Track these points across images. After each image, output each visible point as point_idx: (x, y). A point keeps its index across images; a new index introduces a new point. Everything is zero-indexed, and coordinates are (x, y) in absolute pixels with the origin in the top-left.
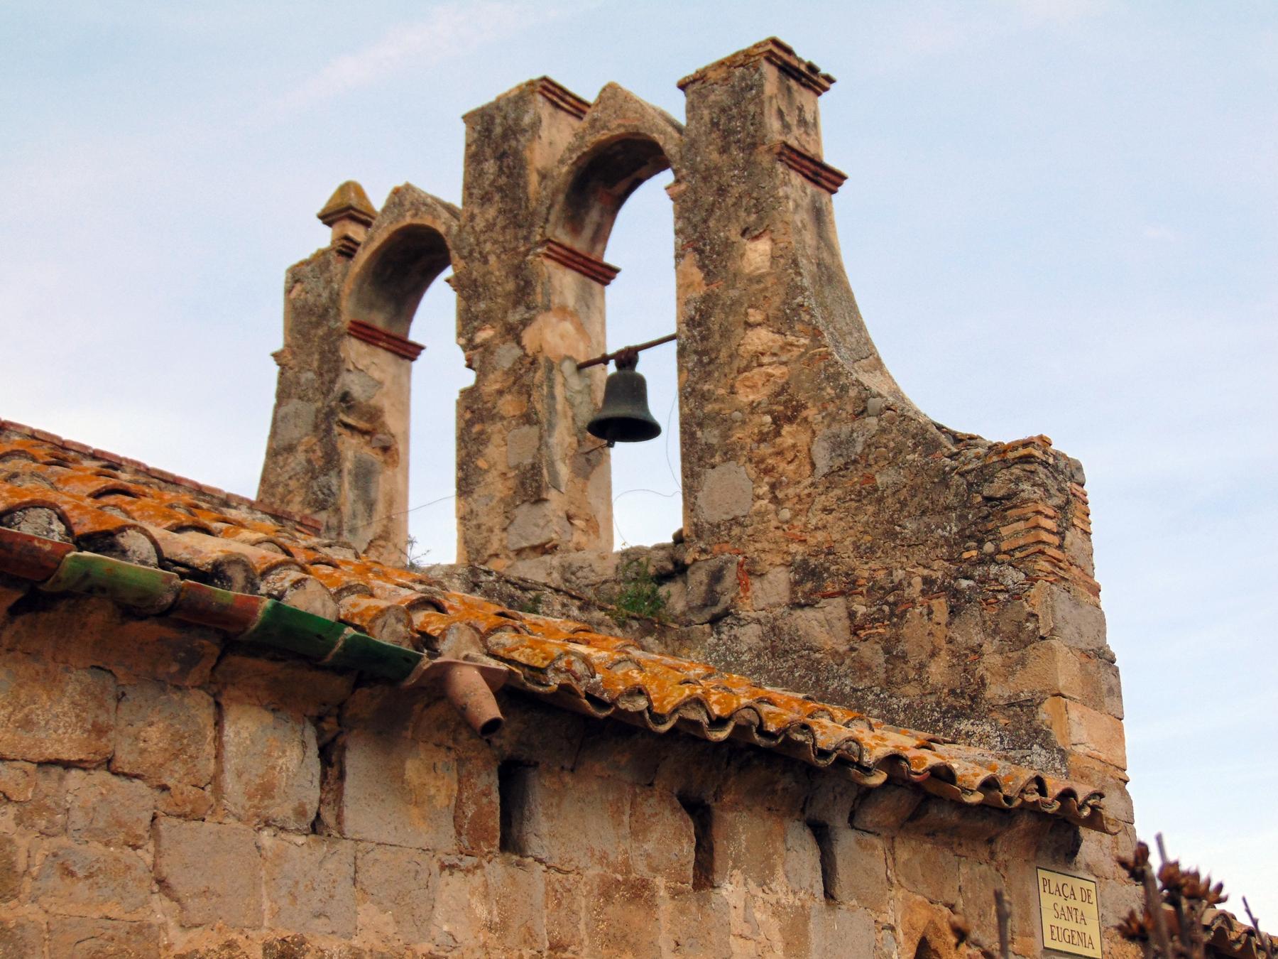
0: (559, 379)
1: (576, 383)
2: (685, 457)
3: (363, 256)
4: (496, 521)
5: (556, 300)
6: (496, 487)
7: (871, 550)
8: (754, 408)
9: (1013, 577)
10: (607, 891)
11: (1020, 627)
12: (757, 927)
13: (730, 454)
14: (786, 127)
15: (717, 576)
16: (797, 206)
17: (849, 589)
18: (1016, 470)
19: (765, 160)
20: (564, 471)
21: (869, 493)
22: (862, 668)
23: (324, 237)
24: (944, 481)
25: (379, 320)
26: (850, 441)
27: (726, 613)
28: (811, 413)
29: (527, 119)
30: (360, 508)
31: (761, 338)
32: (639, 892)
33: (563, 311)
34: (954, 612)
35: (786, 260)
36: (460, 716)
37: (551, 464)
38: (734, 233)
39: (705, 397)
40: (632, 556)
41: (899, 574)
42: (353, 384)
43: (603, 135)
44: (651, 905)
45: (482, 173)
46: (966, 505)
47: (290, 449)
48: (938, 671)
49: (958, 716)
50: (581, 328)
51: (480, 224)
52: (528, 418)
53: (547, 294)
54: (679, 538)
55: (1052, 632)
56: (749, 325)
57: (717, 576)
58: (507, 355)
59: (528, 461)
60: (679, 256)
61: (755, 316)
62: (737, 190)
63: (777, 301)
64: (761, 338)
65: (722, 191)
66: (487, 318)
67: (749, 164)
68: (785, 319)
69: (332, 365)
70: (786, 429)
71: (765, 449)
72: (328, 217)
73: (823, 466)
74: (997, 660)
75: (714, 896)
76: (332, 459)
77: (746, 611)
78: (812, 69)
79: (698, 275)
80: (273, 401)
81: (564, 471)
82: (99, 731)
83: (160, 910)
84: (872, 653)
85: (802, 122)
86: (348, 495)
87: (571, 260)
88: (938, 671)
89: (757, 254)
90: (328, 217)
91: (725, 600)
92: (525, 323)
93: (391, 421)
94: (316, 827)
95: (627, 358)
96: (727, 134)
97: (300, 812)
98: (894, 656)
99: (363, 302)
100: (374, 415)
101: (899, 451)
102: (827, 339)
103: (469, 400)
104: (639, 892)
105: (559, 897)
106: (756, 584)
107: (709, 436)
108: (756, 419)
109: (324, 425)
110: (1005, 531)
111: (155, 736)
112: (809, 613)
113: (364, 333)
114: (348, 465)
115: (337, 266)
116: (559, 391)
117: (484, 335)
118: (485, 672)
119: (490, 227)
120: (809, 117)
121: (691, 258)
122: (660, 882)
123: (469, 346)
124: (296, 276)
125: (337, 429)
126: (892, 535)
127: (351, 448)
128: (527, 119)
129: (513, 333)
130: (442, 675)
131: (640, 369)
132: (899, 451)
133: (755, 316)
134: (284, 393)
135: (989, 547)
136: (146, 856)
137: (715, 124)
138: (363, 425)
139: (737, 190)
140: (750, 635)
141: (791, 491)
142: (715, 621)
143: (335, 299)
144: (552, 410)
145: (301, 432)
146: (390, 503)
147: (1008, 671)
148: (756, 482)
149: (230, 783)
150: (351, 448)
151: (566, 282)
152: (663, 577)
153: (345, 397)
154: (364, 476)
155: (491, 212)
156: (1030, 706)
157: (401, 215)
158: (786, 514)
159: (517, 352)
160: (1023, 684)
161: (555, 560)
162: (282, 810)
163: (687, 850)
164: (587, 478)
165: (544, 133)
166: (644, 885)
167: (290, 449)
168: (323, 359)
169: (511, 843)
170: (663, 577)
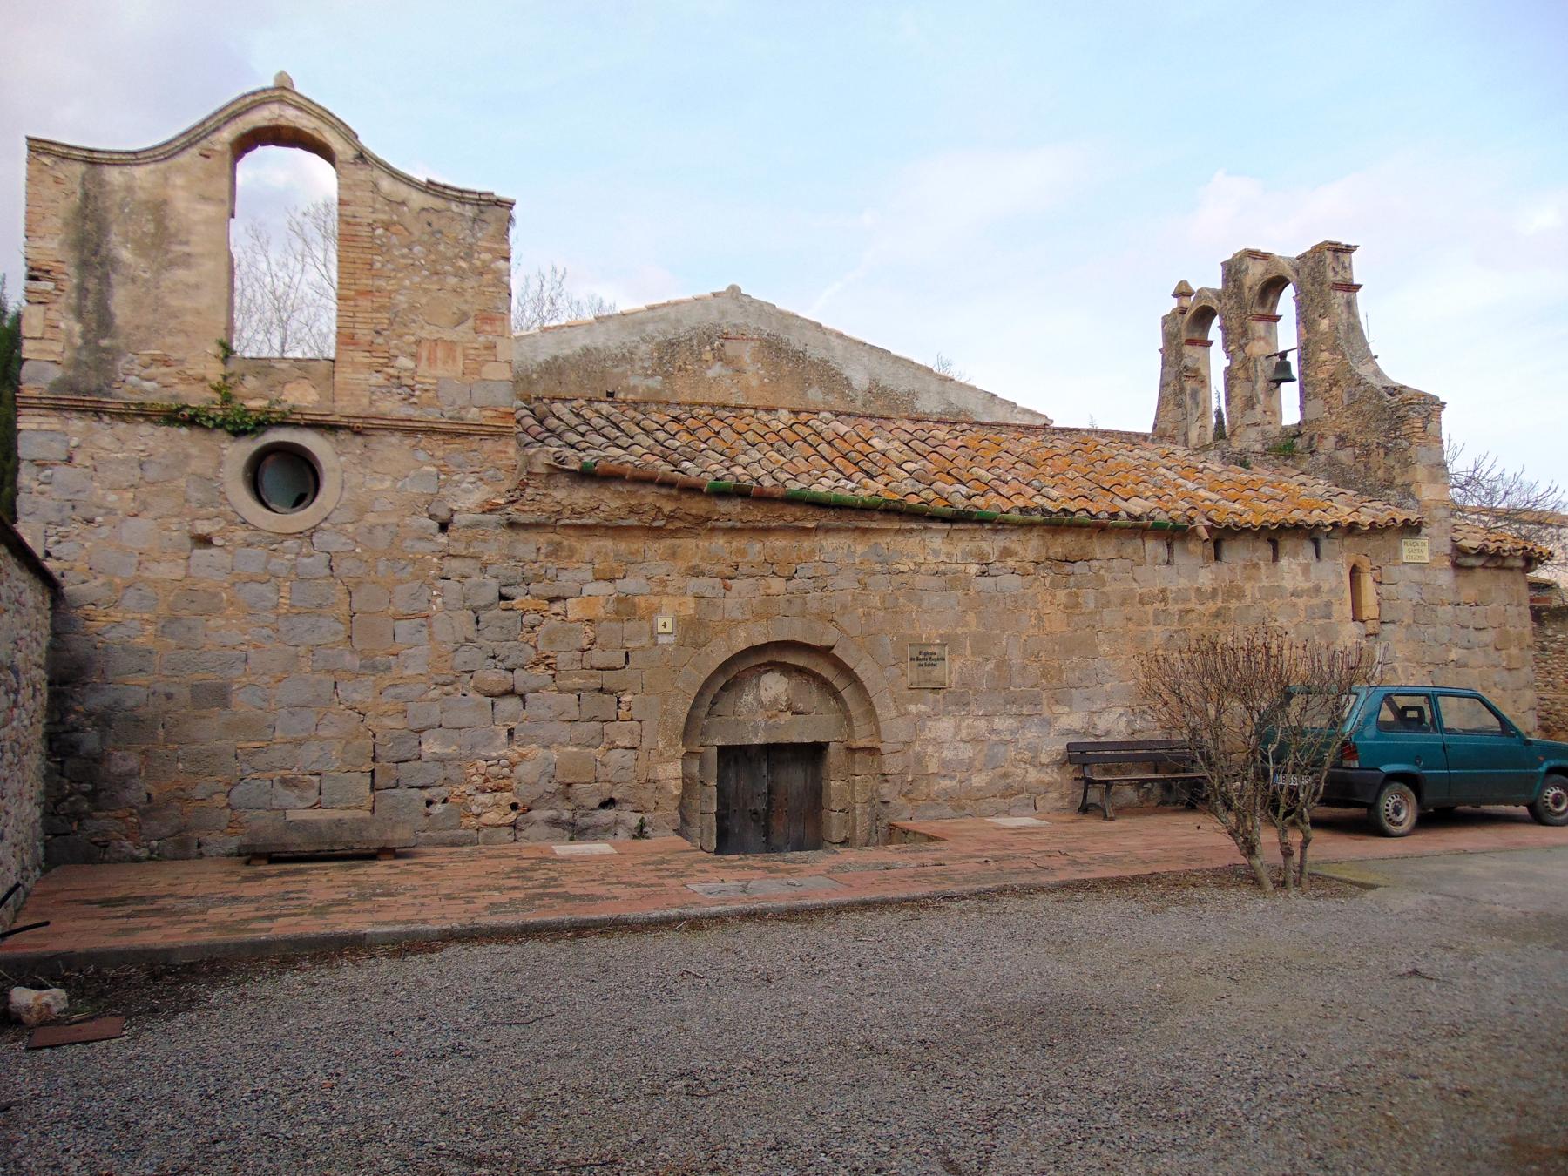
0: (1259, 364)
1: (1266, 363)
2: (1301, 396)
3: (1188, 315)
4: (1239, 415)
5: (1257, 335)
6: (1238, 402)
7: (1361, 432)
8: (1323, 380)
9: (1405, 444)
10: (1245, 567)
11: (1406, 460)
12: (1292, 569)
13: (1316, 396)
14: (1336, 273)
15: (1312, 438)
16: (1339, 305)
17: (1354, 445)
18: (1408, 407)
19: (1327, 290)
20: (1262, 397)
21: (1360, 413)
22: (1357, 471)
23: (1174, 303)
24: (1384, 411)
25: (1196, 336)
26: (1355, 394)
27: (1314, 451)
28: (1342, 383)
29: (1243, 267)
30: (1194, 406)
31: (1325, 356)
32: (1256, 566)
33: (1260, 338)
34: (1386, 454)
35: (1334, 327)
36: (1200, 538)
37: (1257, 395)
38: (1316, 316)
39: (1307, 375)
40: (1285, 428)
41: (1369, 441)
42: (1188, 362)
43: (1270, 276)
44: (1259, 568)
45: (1228, 287)
46: (1391, 418)
47: (1168, 385)
48: (1380, 474)
49: (1387, 488)
50: (1267, 343)
51: (1229, 307)
52: (1248, 379)
53: (1253, 334)
54: (1299, 424)
55: (1416, 463)
56: (1321, 351)
57: (1312, 438)
58: (1240, 356)
59: (1249, 395)
60: (1298, 323)
61: (1324, 348)
62: (1317, 300)
63: (1331, 342)
64: (1325, 356)
65: (1312, 300)
66: (1233, 342)
67: (1322, 291)
68: (1334, 349)
69: (1180, 356)
70: (1334, 388)
71: (1327, 395)
72: (1175, 295)
73: (1346, 403)
74: (1399, 470)
75: (1279, 564)
76: (1182, 390)
77: (1321, 450)
78: (1348, 246)
79: (1304, 331)
80: (1160, 367)
81: (1262, 397)
82: (1119, 551)
83: (1135, 585)
84: (1360, 467)
85: (1344, 268)
86: (1188, 401)
87: (1262, 318)
88: (1380, 474)
89: (1324, 324)
90: (1175, 295)
91: (1314, 446)
92: (1246, 344)
93: (1203, 372)
94: (1168, 563)
95: (1283, 355)
96: (1314, 278)
97: (1164, 561)
98: (1367, 468)
99: (1189, 330)
100: (1197, 371)
101: (1370, 398)
102: (1348, 356)
103: (1228, 370)
104: (1256, 566)
105: (1231, 570)
106: (1325, 441)
107: (1308, 389)
108: (1324, 384)
109: (1179, 376)
110: (1403, 428)
111: (1130, 550)
112: (1341, 452)
113: (1191, 342)
114: (1188, 392)
115: (1179, 318)
116: (1259, 369)
117: (1231, 348)
118: (1206, 527)
119: (1232, 308)
120: (1347, 265)
121: (1302, 324)
122: (1262, 563)
123: (1227, 351)
124: (1165, 320)
125: (1183, 379)
126: (1367, 427)
127: (1189, 385)
128: (1243, 267)
129: (1242, 348)
130: (1194, 530)
131: (1288, 359)
132: (1370, 398)
133: (1324, 348)
134: (1164, 365)
135: (1398, 433)
136: (1131, 575)
137: (1309, 275)
138: (1193, 375)
139: (1317, 300)
140: (1323, 458)
141: (1335, 410)
142: (1311, 453)
143: (1179, 331)
144: (1257, 376)
145: (1170, 379)
146: (1205, 401)
147: (1402, 474)
148: (1324, 406)
149: (1147, 557)
150: (1189, 385)
151: (1260, 327)
152: (1295, 437)
153: (1185, 367)
154: (1194, 394)
155: (1232, 303)
156: (1409, 485)
157: (1201, 302)
158: (1334, 418)
159: (1243, 355)
160: (1406, 479)
161: (1259, 428)
162: (1160, 561)
163: (1270, 553)
164: (1271, 396)
165: (1250, 272)
166: (1257, 564)
167: (1168, 385)
168: (1177, 353)
169: (1217, 557)
170: (1295, 437)
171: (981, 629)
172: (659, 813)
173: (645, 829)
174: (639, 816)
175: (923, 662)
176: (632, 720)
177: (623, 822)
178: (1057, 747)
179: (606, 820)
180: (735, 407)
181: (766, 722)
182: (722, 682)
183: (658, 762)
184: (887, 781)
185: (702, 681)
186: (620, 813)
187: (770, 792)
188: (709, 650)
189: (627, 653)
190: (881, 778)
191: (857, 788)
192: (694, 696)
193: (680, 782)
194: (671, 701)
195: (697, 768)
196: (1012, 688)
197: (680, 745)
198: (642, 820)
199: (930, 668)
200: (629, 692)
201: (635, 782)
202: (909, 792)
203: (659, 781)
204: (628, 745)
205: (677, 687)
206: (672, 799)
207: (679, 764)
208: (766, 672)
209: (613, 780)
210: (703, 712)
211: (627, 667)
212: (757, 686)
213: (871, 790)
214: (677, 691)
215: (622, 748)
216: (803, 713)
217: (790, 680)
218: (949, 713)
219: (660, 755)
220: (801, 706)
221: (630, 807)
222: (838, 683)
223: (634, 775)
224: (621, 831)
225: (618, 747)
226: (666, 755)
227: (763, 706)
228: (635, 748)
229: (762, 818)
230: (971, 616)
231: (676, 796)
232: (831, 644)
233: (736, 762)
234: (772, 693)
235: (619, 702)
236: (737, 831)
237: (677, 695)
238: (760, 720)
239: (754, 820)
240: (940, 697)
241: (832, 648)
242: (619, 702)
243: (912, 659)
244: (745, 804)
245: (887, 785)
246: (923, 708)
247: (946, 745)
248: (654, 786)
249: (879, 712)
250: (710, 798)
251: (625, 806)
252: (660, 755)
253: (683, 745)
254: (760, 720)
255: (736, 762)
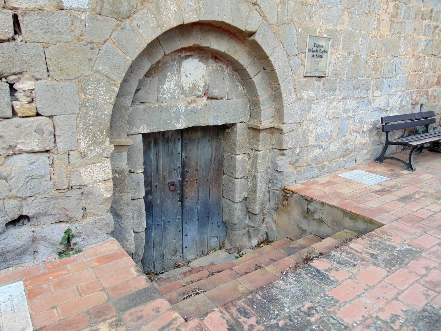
171: (349, 28)
172: (89, 220)
173: (73, 241)
174: (64, 226)
175: (315, 54)
176: (38, 115)
177: (44, 238)
178: (371, 120)
179: (18, 243)
180: (10, 198)
181: (186, 107)
182: (147, 66)
183: (81, 165)
184: (283, 154)
185: (129, 63)
186: (37, 229)
187: (184, 165)
188: (134, 24)
189: (15, 17)
190: (279, 152)
191: (259, 161)
192: (119, 82)
193: (110, 184)
194: (91, 89)
195: (126, 162)
196: (359, 78)
197: (107, 143)
198: (68, 232)
199: (318, 59)
200: (26, 76)
201: (53, 192)
202: (297, 161)
203: (85, 186)
204: (37, 149)
205: (96, 72)
206: (103, 203)
207: (108, 164)
208: (187, 57)
209: (20, 194)
210: (128, 101)
211: (19, 39)
212: (179, 71)
213: (268, 162)
214: (98, 75)
215: (27, 152)
216: (216, 99)
217: (207, 66)
218: (325, 97)
219: (84, 155)
220: (216, 92)
221: (51, 219)
222: (251, 70)
223: (51, 183)
224: (42, 248)
225: (21, 152)
226: (90, 155)
227: (183, 92)
228: (47, 151)
229: (178, 186)
230: (346, 16)
231: (107, 199)
232: (253, 30)
233: (156, 144)
234: (191, 80)
235: (13, 90)
236: (158, 202)
237: (99, 81)
238: (182, 105)
239: (172, 191)
240: (321, 84)
241: (252, 34)
242: (13, 90)
243: (309, 50)
244: (164, 179)
245: (283, 157)
246: (311, 94)
247: (320, 123)
248: (80, 192)
249: (284, 98)
250: (138, 184)
251: (45, 219)
252: (84, 155)
253: (111, 143)
254: (182, 105)
255: (156, 144)
